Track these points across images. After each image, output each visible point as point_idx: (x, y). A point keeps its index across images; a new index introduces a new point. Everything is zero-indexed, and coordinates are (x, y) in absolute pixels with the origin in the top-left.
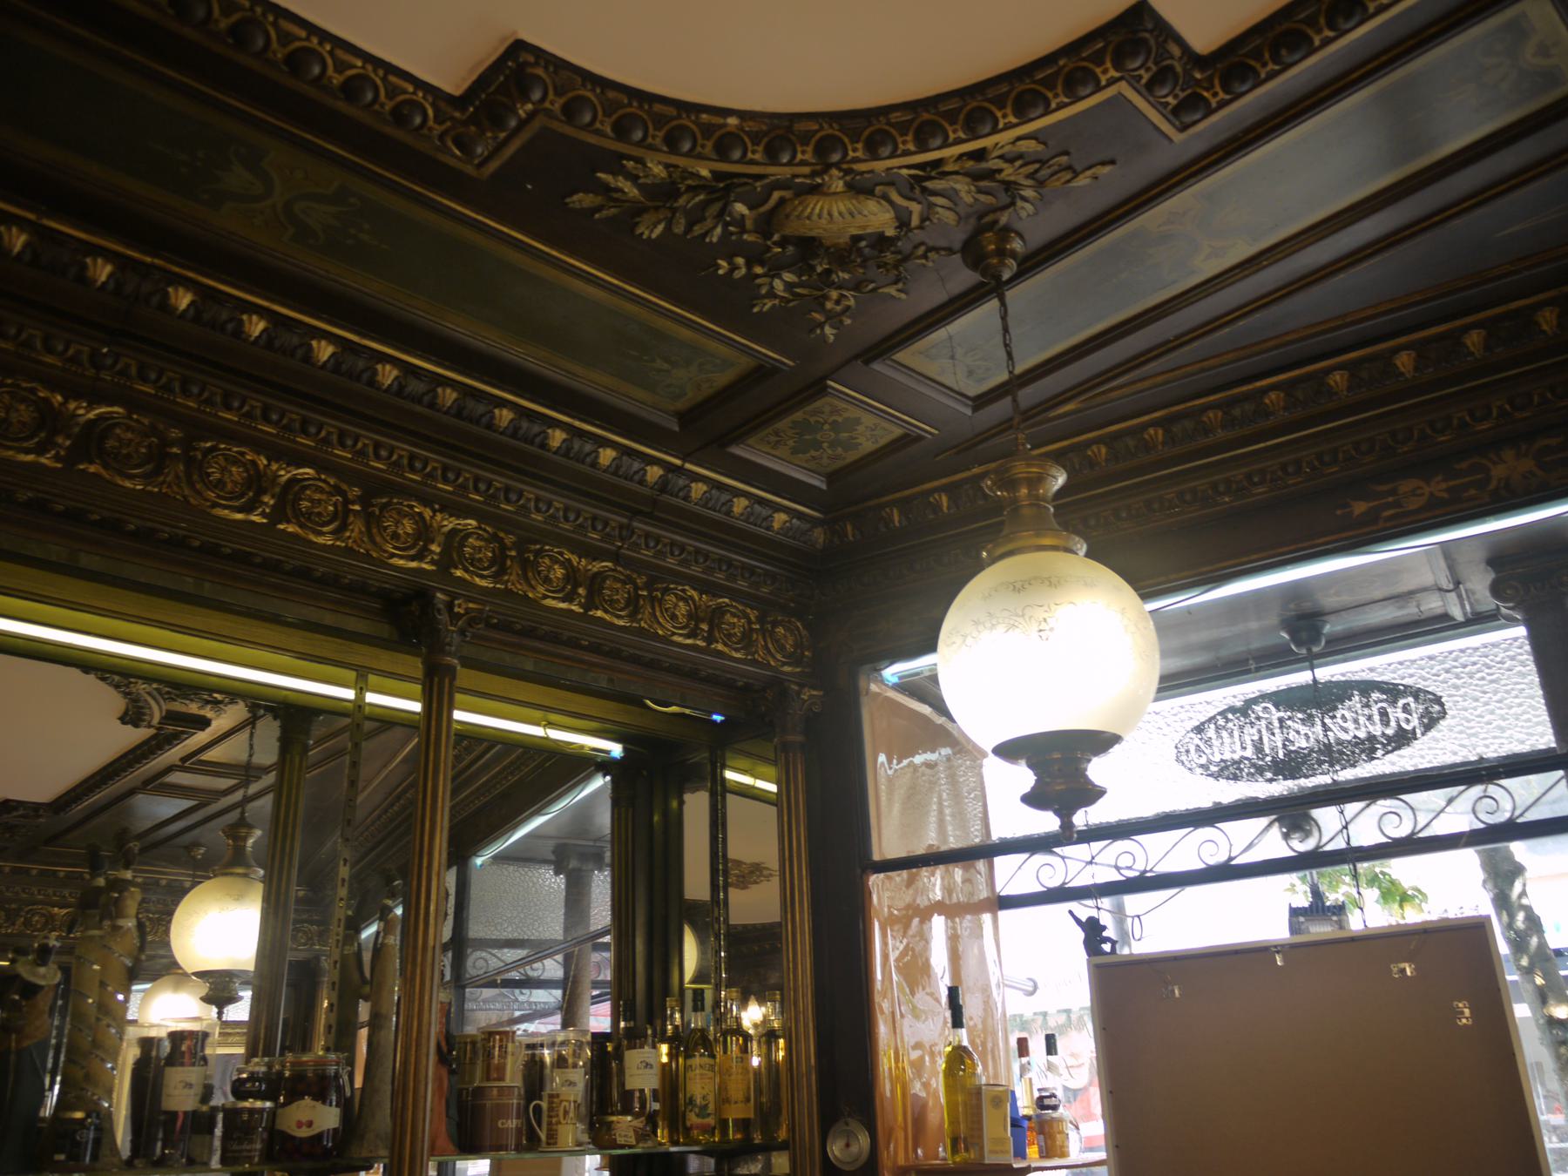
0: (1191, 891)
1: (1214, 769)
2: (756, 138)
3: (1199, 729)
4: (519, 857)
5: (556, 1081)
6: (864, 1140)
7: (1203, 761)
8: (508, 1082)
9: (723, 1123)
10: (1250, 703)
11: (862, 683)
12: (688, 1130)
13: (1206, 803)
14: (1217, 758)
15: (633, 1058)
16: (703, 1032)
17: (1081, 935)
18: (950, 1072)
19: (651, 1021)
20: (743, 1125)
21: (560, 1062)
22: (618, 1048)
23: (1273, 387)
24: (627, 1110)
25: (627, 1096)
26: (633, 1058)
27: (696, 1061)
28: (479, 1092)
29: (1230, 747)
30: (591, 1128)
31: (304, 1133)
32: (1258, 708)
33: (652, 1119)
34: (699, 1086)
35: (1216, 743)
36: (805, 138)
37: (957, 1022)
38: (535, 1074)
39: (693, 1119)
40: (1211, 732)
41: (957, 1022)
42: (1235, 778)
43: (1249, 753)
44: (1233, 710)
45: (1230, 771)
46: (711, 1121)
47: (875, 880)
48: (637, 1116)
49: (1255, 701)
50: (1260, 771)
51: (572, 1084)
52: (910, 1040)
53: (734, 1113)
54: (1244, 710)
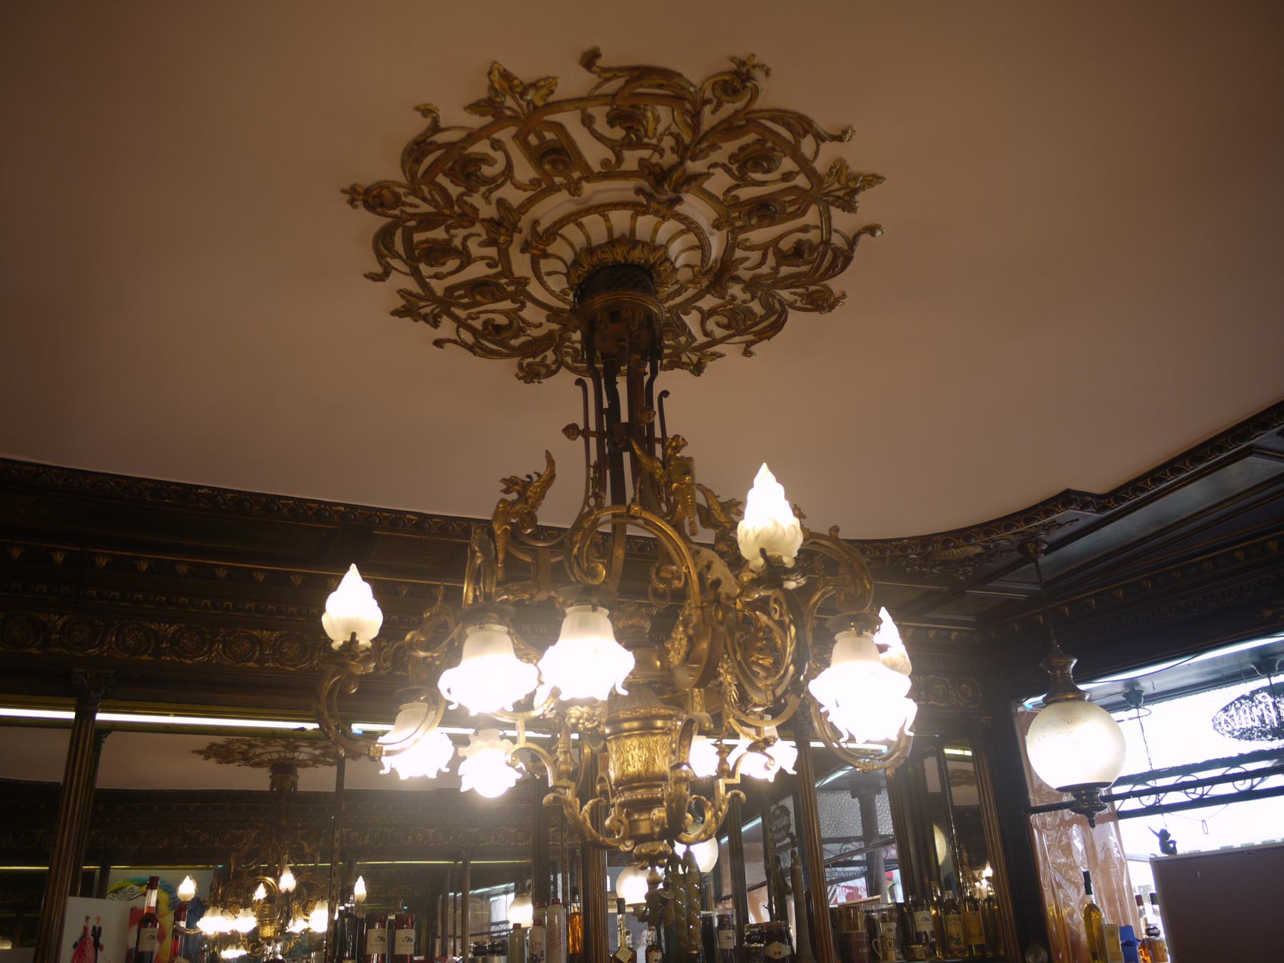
0: (1232, 805)
1: (1236, 733)
2: (916, 545)
3: (1226, 709)
4: (835, 788)
5: (882, 927)
6: (1044, 955)
7: (1230, 729)
8: (860, 930)
9: (970, 948)
10: (1254, 693)
11: (1013, 710)
12: (952, 952)
13: (1235, 754)
14: (1237, 727)
15: (919, 915)
16: (952, 901)
17: (1157, 840)
18: (1088, 917)
19: (925, 897)
20: (980, 948)
21: (884, 919)
22: (909, 909)
23: (1205, 560)
24: (919, 942)
25: (919, 935)
26: (919, 915)
27: (951, 916)
28: (847, 936)
29: (1245, 719)
30: (902, 952)
31: (777, 957)
32: (1259, 697)
33: (932, 946)
34: (954, 929)
35: (1236, 718)
36: (937, 542)
37: (1088, 892)
38: (870, 922)
39: (953, 945)
40: (1233, 711)
41: (1088, 892)
42: (1250, 739)
43: (1257, 723)
44: (1244, 697)
45: (1246, 734)
46: (962, 946)
47: (1035, 819)
48: (924, 945)
49: (1257, 692)
50: (1264, 734)
51: (890, 930)
52: (1065, 903)
53: (975, 942)
54: (1251, 697)
